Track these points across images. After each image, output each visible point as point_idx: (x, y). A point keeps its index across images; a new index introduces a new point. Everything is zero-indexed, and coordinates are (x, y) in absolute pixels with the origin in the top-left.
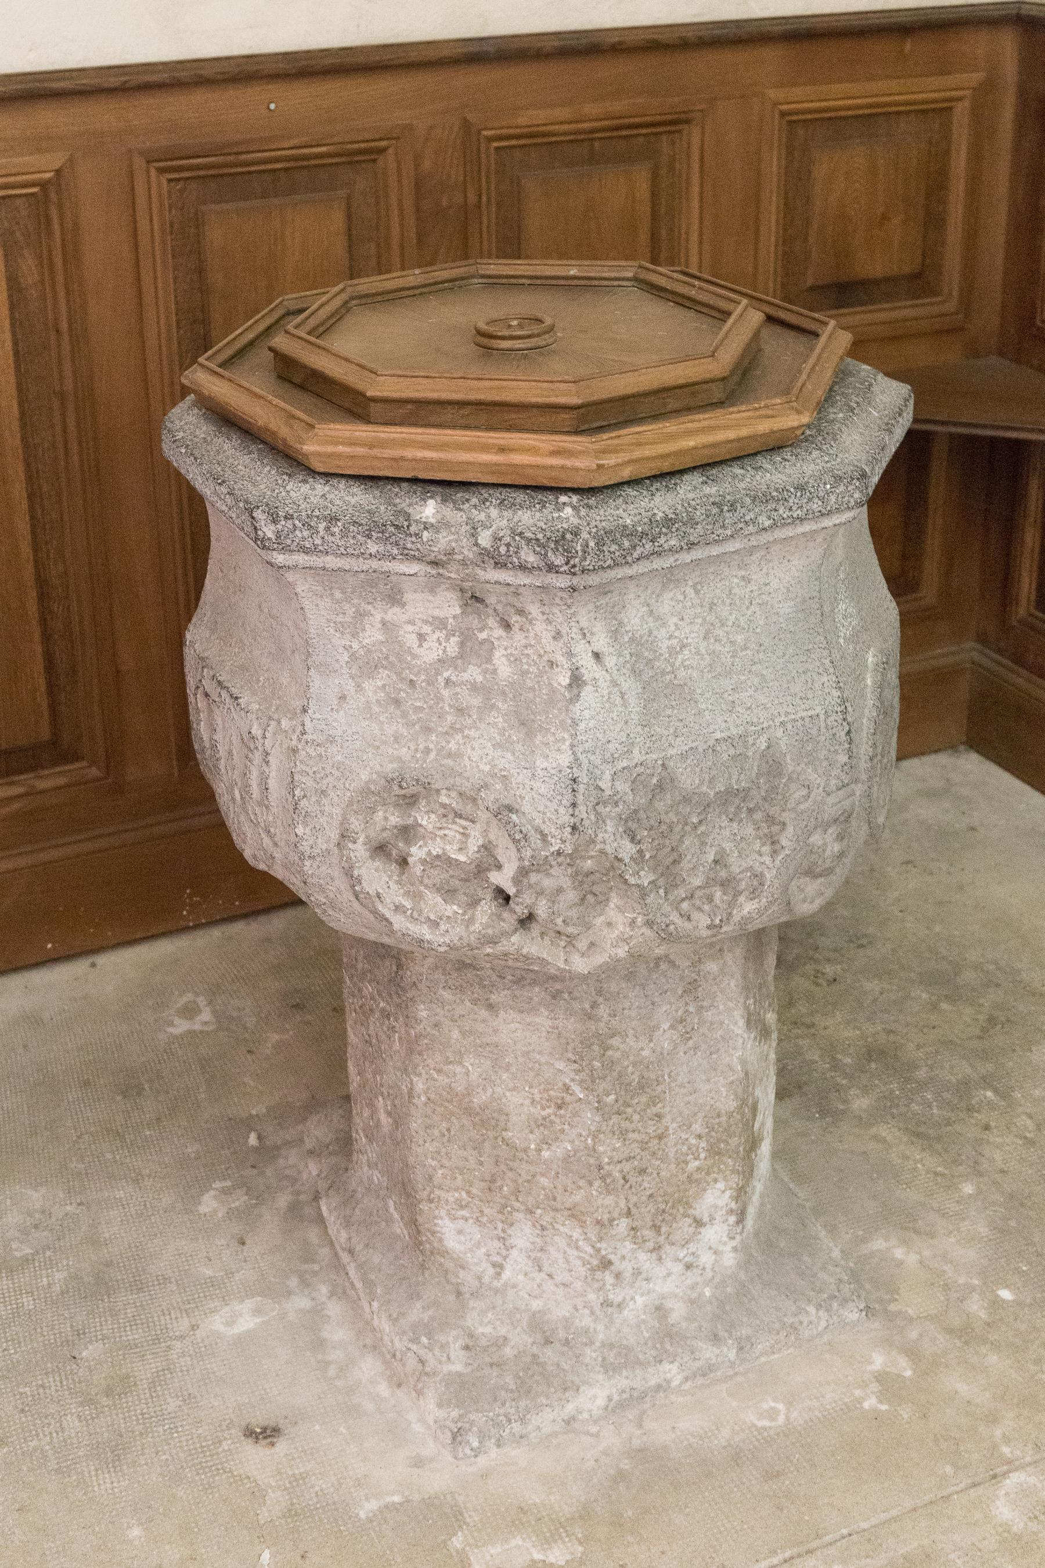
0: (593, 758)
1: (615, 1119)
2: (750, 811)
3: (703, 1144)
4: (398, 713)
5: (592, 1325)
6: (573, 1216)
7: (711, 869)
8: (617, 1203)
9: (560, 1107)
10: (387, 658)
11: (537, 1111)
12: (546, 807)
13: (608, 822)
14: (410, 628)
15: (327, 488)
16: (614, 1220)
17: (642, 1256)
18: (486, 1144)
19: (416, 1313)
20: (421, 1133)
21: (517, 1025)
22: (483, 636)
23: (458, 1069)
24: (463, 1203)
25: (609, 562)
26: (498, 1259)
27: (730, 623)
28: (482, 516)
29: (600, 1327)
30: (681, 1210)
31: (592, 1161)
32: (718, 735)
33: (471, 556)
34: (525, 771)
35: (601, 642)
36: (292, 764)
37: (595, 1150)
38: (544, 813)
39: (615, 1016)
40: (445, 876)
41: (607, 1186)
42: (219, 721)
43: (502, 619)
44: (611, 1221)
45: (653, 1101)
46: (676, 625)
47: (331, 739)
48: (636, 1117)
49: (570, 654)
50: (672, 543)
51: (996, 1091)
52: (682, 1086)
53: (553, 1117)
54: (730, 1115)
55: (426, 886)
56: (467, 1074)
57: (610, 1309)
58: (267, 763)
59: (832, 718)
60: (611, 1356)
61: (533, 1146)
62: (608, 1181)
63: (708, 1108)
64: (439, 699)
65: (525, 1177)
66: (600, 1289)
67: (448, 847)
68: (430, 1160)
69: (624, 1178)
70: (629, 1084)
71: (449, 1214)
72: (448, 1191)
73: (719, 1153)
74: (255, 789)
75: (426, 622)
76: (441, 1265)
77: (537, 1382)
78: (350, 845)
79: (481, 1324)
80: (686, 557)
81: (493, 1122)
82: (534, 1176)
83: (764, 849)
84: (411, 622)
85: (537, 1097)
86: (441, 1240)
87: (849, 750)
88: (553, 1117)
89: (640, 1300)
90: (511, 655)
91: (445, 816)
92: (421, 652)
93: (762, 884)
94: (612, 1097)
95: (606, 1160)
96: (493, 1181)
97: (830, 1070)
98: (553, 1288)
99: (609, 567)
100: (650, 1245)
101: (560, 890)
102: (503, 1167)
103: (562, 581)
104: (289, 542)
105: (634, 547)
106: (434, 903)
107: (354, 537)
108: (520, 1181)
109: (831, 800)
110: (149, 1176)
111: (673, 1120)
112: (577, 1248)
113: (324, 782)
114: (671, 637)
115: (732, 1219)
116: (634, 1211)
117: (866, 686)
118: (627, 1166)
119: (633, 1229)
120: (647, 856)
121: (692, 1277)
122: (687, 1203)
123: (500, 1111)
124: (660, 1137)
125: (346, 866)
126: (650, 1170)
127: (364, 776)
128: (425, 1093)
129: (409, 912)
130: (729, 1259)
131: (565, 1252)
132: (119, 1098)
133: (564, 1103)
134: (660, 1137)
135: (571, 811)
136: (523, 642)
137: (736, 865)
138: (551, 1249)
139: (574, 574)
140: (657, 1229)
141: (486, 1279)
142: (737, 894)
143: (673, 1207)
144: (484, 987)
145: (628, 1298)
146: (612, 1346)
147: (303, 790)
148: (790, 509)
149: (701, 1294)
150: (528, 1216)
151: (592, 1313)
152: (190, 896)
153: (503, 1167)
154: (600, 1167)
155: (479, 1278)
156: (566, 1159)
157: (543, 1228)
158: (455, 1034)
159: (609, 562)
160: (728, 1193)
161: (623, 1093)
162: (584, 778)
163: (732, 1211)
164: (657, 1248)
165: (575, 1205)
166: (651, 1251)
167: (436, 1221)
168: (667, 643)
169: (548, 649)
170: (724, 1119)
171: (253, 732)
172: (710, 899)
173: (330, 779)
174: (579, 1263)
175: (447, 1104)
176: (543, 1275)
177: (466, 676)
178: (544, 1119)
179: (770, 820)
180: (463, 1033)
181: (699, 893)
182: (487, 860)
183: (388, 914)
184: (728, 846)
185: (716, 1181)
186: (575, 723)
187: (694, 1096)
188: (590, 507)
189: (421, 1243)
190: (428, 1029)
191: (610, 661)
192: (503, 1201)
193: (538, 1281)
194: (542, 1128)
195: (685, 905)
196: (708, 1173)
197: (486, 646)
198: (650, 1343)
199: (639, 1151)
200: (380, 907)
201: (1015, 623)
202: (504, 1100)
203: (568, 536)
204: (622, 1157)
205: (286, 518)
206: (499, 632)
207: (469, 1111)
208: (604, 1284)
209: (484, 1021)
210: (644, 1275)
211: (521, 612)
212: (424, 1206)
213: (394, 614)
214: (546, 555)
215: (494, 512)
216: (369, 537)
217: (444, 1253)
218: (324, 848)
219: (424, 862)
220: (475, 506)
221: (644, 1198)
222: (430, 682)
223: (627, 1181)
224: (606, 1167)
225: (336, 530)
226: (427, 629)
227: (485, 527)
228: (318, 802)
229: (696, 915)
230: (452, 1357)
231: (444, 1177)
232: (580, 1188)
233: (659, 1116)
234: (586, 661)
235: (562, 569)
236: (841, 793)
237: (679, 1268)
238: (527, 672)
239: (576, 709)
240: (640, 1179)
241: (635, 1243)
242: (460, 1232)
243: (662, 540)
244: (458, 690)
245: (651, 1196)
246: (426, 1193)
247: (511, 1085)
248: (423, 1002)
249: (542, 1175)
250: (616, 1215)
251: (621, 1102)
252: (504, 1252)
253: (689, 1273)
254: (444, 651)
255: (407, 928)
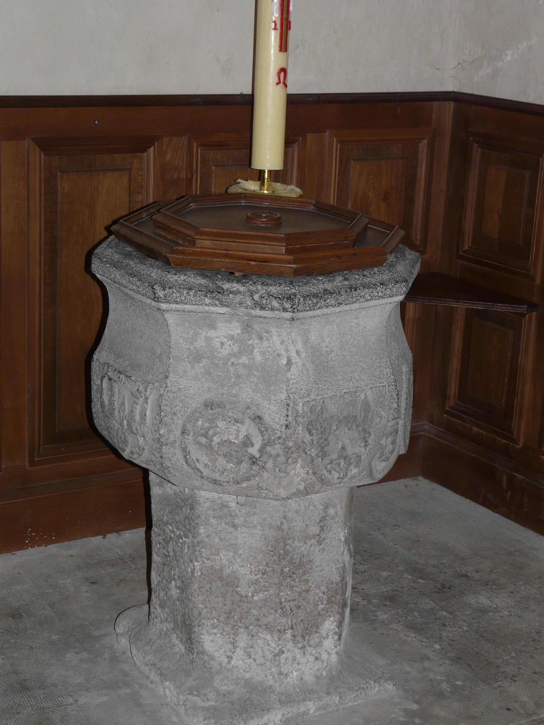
0: (295, 396)
1: (289, 580)
2: (357, 426)
3: (325, 597)
4: (210, 378)
5: (274, 684)
6: (267, 628)
7: (340, 451)
8: (287, 622)
9: (264, 574)
10: (206, 354)
11: (253, 577)
12: (275, 417)
13: (300, 425)
14: (218, 340)
15: (185, 277)
16: (286, 630)
17: (297, 651)
18: (228, 594)
19: (190, 683)
20: (197, 591)
21: (246, 534)
22: (250, 342)
23: (217, 557)
24: (215, 626)
25: (308, 308)
26: (230, 654)
27: (350, 343)
28: (254, 289)
29: (277, 685)
30: (315, 629)
31: (277, 600)
32: (345, 391)
33: (250, 304)
34: (266, 401)
35: (300, 346)
36: (161, 401)
37: (279, 594)
38: (274, 420)
39: (291, 529)
40: (228, 450)
41: (284, 612)
42: (116, 390)
43: (259, 335)
44: (285, 630)
45: (304, 573)
46: (329, 342)
47: (180, 390)
48: (297, 580)
49: (287, 350)
50: (332, 302)
51: (447, 611)
52: (317, 567)
53: (260, 579)
54: (337, 584)
55: (219, 455)
56: (221, 560)
57: (282, 676)
58: (147, 403)
59: (391, 388)
60: (283, 698)
61: (250, 594)
62: (284, 610)
63: (328, 579)
64: (228, 371)
65: (245, 610)
66: (278, 665)
67: (230, 437)
68: (200, 605)
69: (291, 610)
70: (295, 563)
71: (207, 632)
72: (208, 620)
73: (332, 603)
74: (138, 417)
75: (224, 337)
76: (202, 659)
77: (250, 707)
78: (186, 437)
79: (221, 685)
80: (337, 309)
81: (232, 583)
82: (250, 609)
83: (362, 444)
84: (218, 337)
85: (253, 570)
86: (203, 646)
87: (398, 402)
88: (260, 579)
89: (295, 673)
90: (262, 351)
91: (230, 422)
92: (222, 350)
93: (360, 461)
94: (287, 569)
95: (284, 600)
96: (230, 613)
97: (368, 604)
98: (256, 667)
99: (307, 310)
100: (300, 645)
101: (278, 455)
102: (235, 606)
103: (288, 315)
104: (170, 299)
105: (318, 303)
106: (222, 462)
107: (199, 297)
108: (243, 612)
109: (389, 424)
110: (36, 648)
111: (313, 583)
112: (268, 645)
113: (175, 409)
114: (327, 347)
115: (336, 637)
116: (294, 627)
117: (403, 379)
118: (292, 604)
119: (294, 636)
120: (315, 442)
121: (318, 665)
122: (317, 626)
123: (236, 578)
124: (307, 591)
125: (183, 446)
126: (302, 607)
127: (194, 405)
128: (200, 571)
129: (211, 468)
130: (334, 658)
131: (262, 648)
132: (10, 619)
133: (265, 572)
134: (307, 591)
135: (286, 418)
136: (267, 345)
137: (350, 450)
138: (256, 647)
139: (294, 312)
140: (303, 637)
141: (224, 664)
142: (350, 464)
143: (311, 627)
144: (232, 516)
145: (290, 671)
146: (283, 694)
147: (165, 413)
148: (378, 293)
149: (322, 674)
150: (246, 630)
151: (274, 677)
152: (31, 532)
153: (235, 606)
154: (281, 603)
155: (221, 664)
156: (265, 600)
157: (253, 636)
158: (217, 540)
159: (308, 308)
160: (335, 623)
161: (292, 567)
162: (291, 404)
163: (336, 632)
164: (303, 648)
165: (269, 623)
166: (301, 649)
167: (201, 636)
168: (325, 349)
169: (278, 348)
170: (334, 585)
171: (140, 389)
172: (339, 464)
173: (178, 407)
174: (268, 653)
175: (210, 575)
176: (251, 660)
177: (241, 361)
178: (256, 580)
179: (364, 430)
180: (220, 539)
181: (334, 462)
182: (247, 442)
183: (201, 469)
184: (347, 442)
185: (330, 616)
186: (288, 380)
187: (322, 572)
188: (299, 286)
189: (193, 649)
190: (204, 538)
191: (303, 355)
192: (234, 623)
193: (249, 663)
194: (255, 585)
195: (329, 467)
196: (327, 612)
197: (250, 348)
198: (300, 693)
199: (297, 597)
200: (198, 465)
201: (447, 409)
202: (238, 572)
203: (292, 296)
204: (290, 598)
205: (169, 288)
206: (257, 341)
207: (220, 578)
208: (280, 663)
209: (231, 533)
210: (297, 661)
211: (267, 332)
212: (196, 629)
213: (212, 333)
214: (283, 304)
215: (259, 287)
216: (206, 296)
217: (203, 652)
218: (173, 440)
219: (219, 444)
220: (251, 285)
221: (299, 621)
222: (225, 364)
223: (292, 611)
224: (283, 603)
225: (192, 293)
226: (225, 340)
227: (256, 293)
228: (172, 418)
229: (333, 472)
230: (210, 699)
231: (207, 612)
232: (271, 614)
233: (307, 581)
234: (293, 354)
235: (289, 310)
236: (393, 422)
237: (312, 659)
238: (268, 358)
239: (289, 375)
240: (298, 611)
241: (294, 644)
242: (212, 641)
243: (328, 301)
244: (237, 367)
245: (302, 620)
246: (197, 622)
247: (241, 564)
248: (203, 525)
249: (254, 608)
250: (286, 627)
251: (291, 572)
252: (233, 650)
253: (316, 663)
254: (232, 350)
255: (209, 475)
